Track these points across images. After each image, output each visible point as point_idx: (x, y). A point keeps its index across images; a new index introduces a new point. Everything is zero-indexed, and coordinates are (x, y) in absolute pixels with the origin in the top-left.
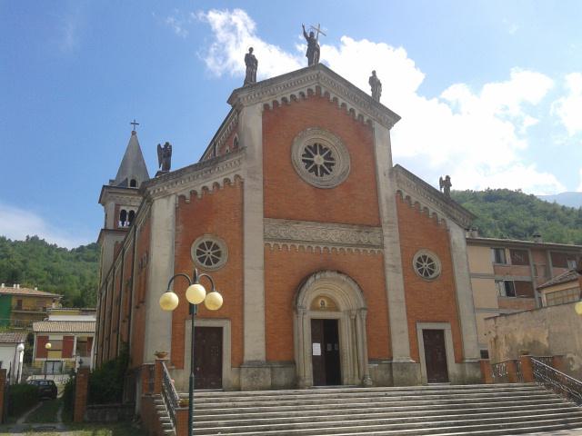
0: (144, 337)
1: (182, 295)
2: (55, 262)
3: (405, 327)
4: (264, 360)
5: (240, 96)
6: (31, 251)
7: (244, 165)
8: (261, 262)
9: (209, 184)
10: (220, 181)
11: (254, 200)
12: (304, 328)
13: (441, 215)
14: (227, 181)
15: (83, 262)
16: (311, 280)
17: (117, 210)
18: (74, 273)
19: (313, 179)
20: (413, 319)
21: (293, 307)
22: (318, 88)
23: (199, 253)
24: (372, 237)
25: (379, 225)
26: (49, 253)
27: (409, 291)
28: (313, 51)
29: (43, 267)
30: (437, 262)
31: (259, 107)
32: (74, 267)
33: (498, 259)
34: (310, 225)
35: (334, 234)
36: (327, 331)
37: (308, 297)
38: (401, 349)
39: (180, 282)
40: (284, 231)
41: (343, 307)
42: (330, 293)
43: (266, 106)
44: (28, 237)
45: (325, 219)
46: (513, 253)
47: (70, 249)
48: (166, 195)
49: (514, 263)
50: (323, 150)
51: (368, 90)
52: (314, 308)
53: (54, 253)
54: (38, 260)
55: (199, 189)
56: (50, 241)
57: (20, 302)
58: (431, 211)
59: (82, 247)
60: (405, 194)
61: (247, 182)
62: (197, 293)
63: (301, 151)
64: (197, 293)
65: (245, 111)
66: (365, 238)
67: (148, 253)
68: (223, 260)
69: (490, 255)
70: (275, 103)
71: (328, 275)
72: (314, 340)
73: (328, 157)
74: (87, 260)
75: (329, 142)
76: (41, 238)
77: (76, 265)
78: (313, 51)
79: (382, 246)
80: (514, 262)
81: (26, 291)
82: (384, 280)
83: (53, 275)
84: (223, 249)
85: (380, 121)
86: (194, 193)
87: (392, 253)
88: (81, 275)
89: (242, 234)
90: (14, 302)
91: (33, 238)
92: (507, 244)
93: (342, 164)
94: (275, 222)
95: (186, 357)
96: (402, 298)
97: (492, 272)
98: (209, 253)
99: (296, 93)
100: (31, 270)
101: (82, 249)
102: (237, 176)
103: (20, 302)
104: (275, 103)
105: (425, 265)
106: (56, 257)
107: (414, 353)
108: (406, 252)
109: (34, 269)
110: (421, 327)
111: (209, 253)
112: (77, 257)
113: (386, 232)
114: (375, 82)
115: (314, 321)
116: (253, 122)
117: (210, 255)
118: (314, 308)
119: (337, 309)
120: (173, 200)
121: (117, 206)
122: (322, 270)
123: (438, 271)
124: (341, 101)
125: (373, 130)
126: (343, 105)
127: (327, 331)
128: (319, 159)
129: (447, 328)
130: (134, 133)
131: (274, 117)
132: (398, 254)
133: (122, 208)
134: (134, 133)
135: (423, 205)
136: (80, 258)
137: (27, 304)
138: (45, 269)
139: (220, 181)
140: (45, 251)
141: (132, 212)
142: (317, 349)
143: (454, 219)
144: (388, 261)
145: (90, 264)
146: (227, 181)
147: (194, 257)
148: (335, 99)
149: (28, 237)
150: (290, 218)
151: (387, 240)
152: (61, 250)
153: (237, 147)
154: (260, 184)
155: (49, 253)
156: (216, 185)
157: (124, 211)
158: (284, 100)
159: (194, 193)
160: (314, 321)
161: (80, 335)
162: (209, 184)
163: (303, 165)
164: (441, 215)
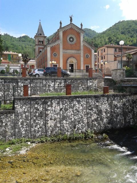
2: (13, 42)
3: (83, 65)
4: (48, 67)
6: (6, 38)
7: (60, 41)
8: (62, 56)
11: (61, 47)
12: (68, 65)
13: (90, 48)
14: (57, 44)
17: (38, 40)
18: (19, 46)
19: (70, 43)
20: (84, 64)
21: (67, 62)
22: (72, 27)
23: (54, 55)
24: (79, 52)
25: (80, 50)
26: (11, 39)
27: (84, 60)
28: (71, 20)
29: (10, 44)
31: (62, 32)
32: (19, 44)
33: (115, 51)
34: (70, 50)
35: (73, 52)
36: (72, 66)
38: (82, 68)
39: (51, 61)
40: (66, 51)
44: (4, 34)
46: (119, 49)
53: (13, 39)
55: (53, 45)
56: (11, 35)
57: (13, 56)
58: (89, 47)
59: (21, 37)
64: (53, 62)
65: (60, 32)
66: (78, 52)
68: (57, 56)
69: (113, 50)
71: (72, 58)
73: (73, 39)
74: (22, 41)
75: (73, 36)
76: (8, 34)
77: (20, 43)
78: (71, 20)
79: (80, 53)
80: (119, 51)
81: (13, 53)
83: (14, 46)
84: (57, 54)
86: (53, 46)
87: (82, 54)
89: (59, 52)
91: (6, 34)
94: (64, 50)
95: (81, 63)
97: (114, 53)
98: (55, 55)
99: (68, 29)
100: (7, 45)
101: (20, 38)
103: (13, 56)
106: (13, 40)
108: (84, 54)
110: (85, 65)
111: (55, 55)
112: (20, 40)
113: (81, 51)
114: (81, 25)
115: (70, 64)
116: (61, 34)
118: (70, 62)
120: (50, 47)
121: (38, 39)
122: (71, 57)
123: (89, 57)
127: (72, 66)
128: (71, 40)
129: (90, 65)
130: (40, 23)
132: (83, 54)
133: (39, 40)
134: (40, 23)
136: (20, 41)
137: (14, 57)
138: (11, 44)
140: (10, 38)
142: (70, 68)
143: (93, 49)
144: (81, 56)
145: (23, 42)
146: (57, 44)
147: (53, 55)
149: (4, 34)
151: (81, 52)
152: (14, 38)
153: (58, 38)
155: (11, 39)
156: (56, 45)
157: (39, 41)
158: (66, 30)
160: (70, 64)
161: (30, 64)
163: (69, 41)
164: (90, 48)
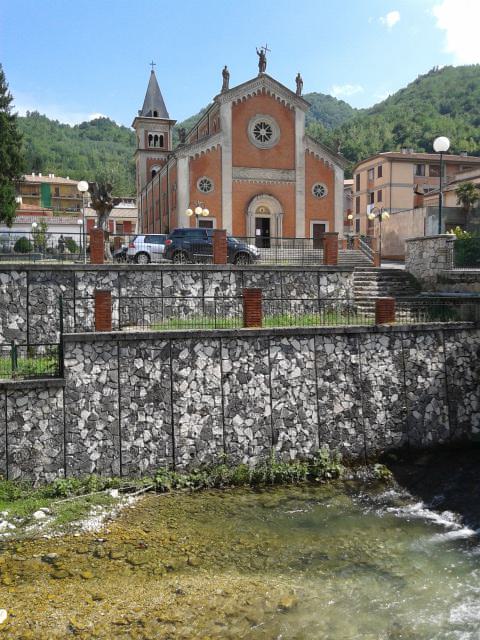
0: (177, 219)
1: (194, 211)
2: (59, 140)
3: (304, 222)
5: (220, 98)
9: (205, 150)
10: (210, 148)
11: (227, 157)
12: (252, 223)
15: (88, 140)
16: (255, 199)
19: (258, 144)
20: (308, 218)
21: (246, 212)
22: (264, 89)
26: (52, 130)
27: (308, 205)
28: (262, 63)
29: (49, 146)
30: (326, 189)
31: (230, 104)
33: (419, 173)
34: (257, 170)
35: (270, 174)
36: (264, 224)
37: (253, 208)
38: (300, 232)
39: (192, 206)
40: (243, 173)
41: (272, 212)
42: (266, 205)
43: (234, 103)
44: (28, 112)
45: (263, 167)
46: (431, 167)
47: (72, 125)
48: (184, 157)
49: (430, 176)
50: (265, 126)
51: (293, 88)
52: (257, 213)
53: (57, 130)
54: (42, 139)
56: (52, 117)
57: (57, 190)
59: (85, 123)
60: (311, 151)
61: (224, 148)
62: (199, 210)
63: (253, 128)
64: (199, 210)
67: (176, 183)
68: (212, 189)
69: (411, 169)
70: (239, 100)
72: (257, 227)
74: (91, 139)
80: (431, 175)
81: (60, 180)
82: (295, 198)
83: (62, 156)
85: (300, 108)
86: (197, 155)
88: (88, 156)
90: (53, 190)
91: (33, 114)
92: (426, 161)
93: (276, 134)
94: (238, 169)
96: (303, 207)
99: (251, 94)
100: (39, 150)
101: (84, 126)
102: (219, 145)
103: (57, 190)
104: (239, 100)
105: (319, 190)
107: (307, 233)
109: (42, 149)
112: (81, 135)
113: (298, 173)
114: (299, 81)
115: (257, 219)
116: (227, 113)
117: (206, 186)
118: (257, 213)
119: (269, 213)
121: (146, 132)
122: (252, 200)
123: (325, 194)
124: (277, 96)
125: (295, 112)
126: (279, 98)
127: (264, 224)
130: (153, 72)
131: (237, 109)
134: (153, 72)
135: (321, 156)
139: (210, 148)
140: (48, 128)
141: (161, 137)
142: (259, 232)
143: (338, 164)
144: (298, 189)
148: (274, 95)
149: (28, 112)
150: (246, 167)
152: (63, 126)
153: (217, 128)
154: (230, 149)
155: (52, 130)
158: (244, 98)
159: (197, 155)
160: (257, 219)
162: (205, 150)
